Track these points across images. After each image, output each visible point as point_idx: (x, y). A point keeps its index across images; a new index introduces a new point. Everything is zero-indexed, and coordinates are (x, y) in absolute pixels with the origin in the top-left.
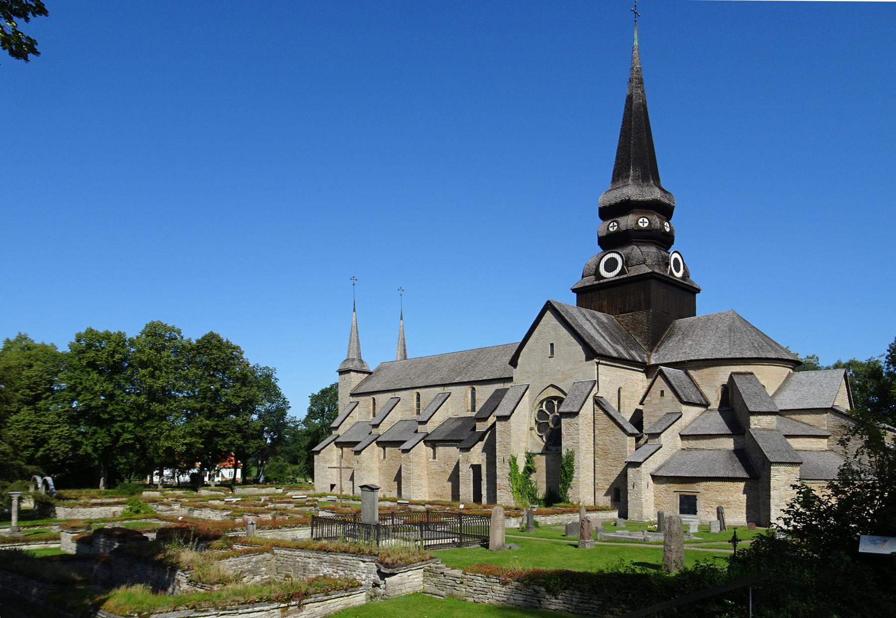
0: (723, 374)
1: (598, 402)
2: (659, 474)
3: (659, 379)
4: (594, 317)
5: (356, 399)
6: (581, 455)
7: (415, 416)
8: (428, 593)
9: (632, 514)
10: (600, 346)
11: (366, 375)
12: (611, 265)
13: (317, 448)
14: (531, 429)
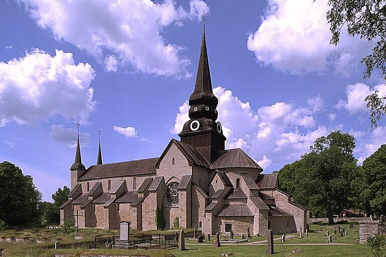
12: (195, 126)
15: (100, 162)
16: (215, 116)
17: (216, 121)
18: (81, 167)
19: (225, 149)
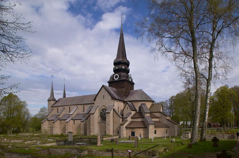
0: (139, 104)
1: (114, 110)
2: (127, 127)
3: (127, 105)
4: (113, 89)
5: (53, 108)
6: (111, 123)
7: (83, 113)
8: (218, 21)
9: (122, 137)
10: (114, 96)
11: (55, 102)
12: (116, 77)
13: (42, 122)
14: (99, 116)
15: (65, 96)
16: (128, 71)
17: (129, 74)
18: (54, 100)
19: (134, 89)
